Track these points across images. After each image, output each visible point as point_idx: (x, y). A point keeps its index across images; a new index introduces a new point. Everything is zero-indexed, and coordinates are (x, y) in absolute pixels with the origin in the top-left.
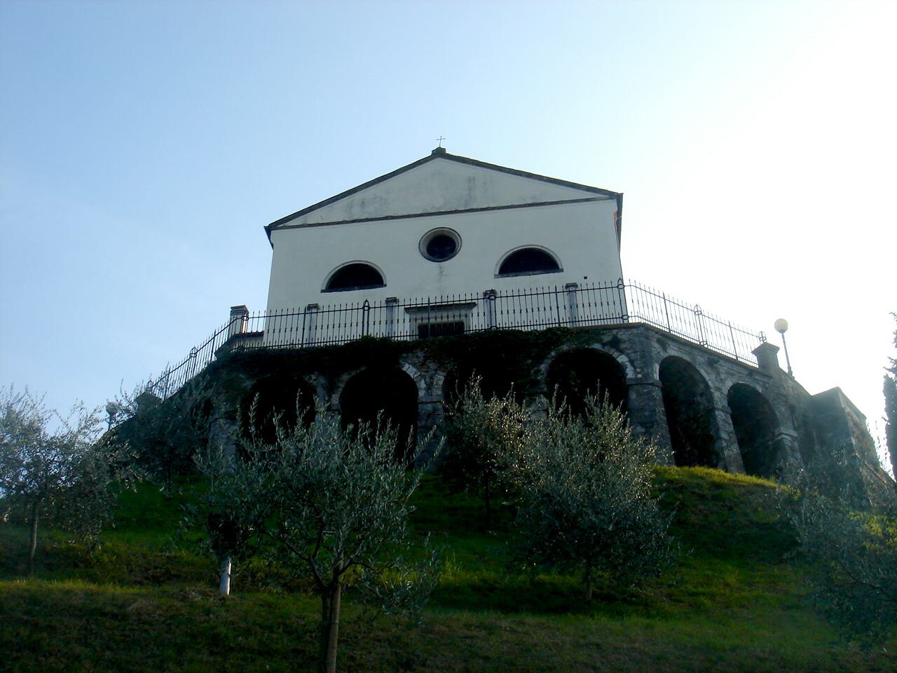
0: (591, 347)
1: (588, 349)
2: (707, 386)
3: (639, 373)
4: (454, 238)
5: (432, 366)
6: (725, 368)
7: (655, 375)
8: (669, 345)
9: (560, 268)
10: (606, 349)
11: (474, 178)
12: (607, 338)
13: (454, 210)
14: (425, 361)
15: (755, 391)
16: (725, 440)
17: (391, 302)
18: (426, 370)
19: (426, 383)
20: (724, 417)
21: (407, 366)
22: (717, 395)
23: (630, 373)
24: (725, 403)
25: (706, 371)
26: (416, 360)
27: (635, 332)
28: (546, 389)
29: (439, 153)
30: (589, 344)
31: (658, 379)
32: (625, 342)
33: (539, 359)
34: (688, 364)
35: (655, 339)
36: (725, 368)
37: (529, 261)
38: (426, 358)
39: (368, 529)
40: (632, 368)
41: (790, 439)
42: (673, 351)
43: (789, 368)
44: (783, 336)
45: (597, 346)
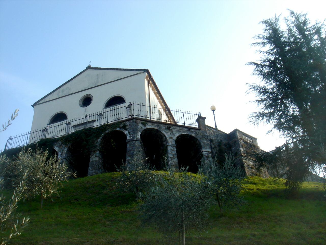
0: (116, 130)
1: (115, 131)
2: (166, 138)
3: (131, 137)
4: (90, 97)
5: (64, 146)
6: (176, 129)
7: (138, 137)
8: (147, 124)
9: (125, 101)
10: (121, 130)
11: (99, 75)
12: (121, 126)
13: (91, 87)
14: (61, 144)
15: (191, 136)
16: (170, 157)
17: (69, 124)
18: (62, 148)
19: (61, 152)
20: (172, 149)
21: (56, 147)
22: (170, 140)
23: (128, 137)
24: (174, 143)
25: (165, 132)
26: (58, 145)
27: (132, 121)
28: (99, 148)
29: (89, 68)
30: (115, 129)
31: (139, 138)
32: (128, 126)
33: (97, 137)
34: (157, 130)
35: (141, 123)
36: (176, 129)
37: (116, 101)
38: (62, 143)
39: (239, 190)
40: (129, 135)
41: (207, 153)
42: (149, 126)
43: (216, 126)
44: (214, 113)
45: (118, 129)
